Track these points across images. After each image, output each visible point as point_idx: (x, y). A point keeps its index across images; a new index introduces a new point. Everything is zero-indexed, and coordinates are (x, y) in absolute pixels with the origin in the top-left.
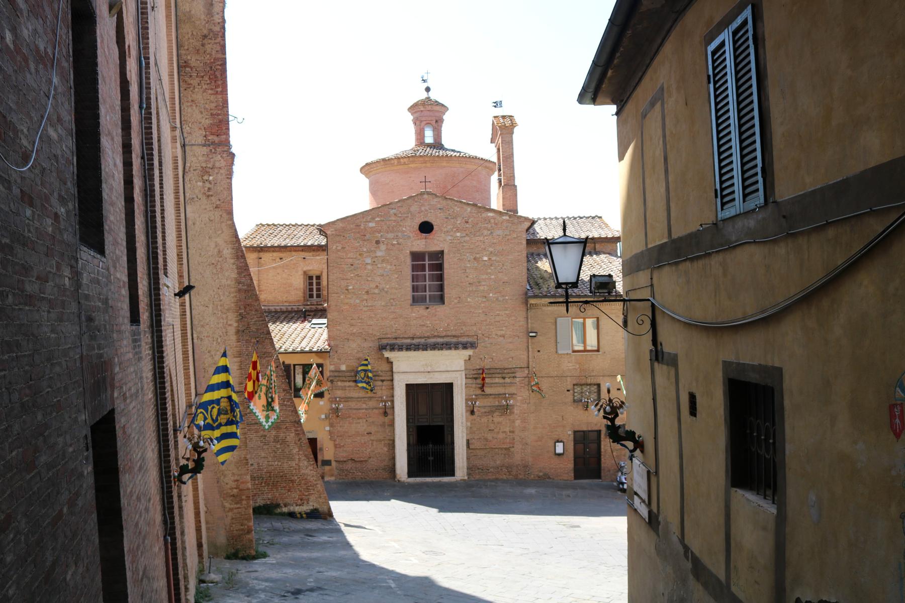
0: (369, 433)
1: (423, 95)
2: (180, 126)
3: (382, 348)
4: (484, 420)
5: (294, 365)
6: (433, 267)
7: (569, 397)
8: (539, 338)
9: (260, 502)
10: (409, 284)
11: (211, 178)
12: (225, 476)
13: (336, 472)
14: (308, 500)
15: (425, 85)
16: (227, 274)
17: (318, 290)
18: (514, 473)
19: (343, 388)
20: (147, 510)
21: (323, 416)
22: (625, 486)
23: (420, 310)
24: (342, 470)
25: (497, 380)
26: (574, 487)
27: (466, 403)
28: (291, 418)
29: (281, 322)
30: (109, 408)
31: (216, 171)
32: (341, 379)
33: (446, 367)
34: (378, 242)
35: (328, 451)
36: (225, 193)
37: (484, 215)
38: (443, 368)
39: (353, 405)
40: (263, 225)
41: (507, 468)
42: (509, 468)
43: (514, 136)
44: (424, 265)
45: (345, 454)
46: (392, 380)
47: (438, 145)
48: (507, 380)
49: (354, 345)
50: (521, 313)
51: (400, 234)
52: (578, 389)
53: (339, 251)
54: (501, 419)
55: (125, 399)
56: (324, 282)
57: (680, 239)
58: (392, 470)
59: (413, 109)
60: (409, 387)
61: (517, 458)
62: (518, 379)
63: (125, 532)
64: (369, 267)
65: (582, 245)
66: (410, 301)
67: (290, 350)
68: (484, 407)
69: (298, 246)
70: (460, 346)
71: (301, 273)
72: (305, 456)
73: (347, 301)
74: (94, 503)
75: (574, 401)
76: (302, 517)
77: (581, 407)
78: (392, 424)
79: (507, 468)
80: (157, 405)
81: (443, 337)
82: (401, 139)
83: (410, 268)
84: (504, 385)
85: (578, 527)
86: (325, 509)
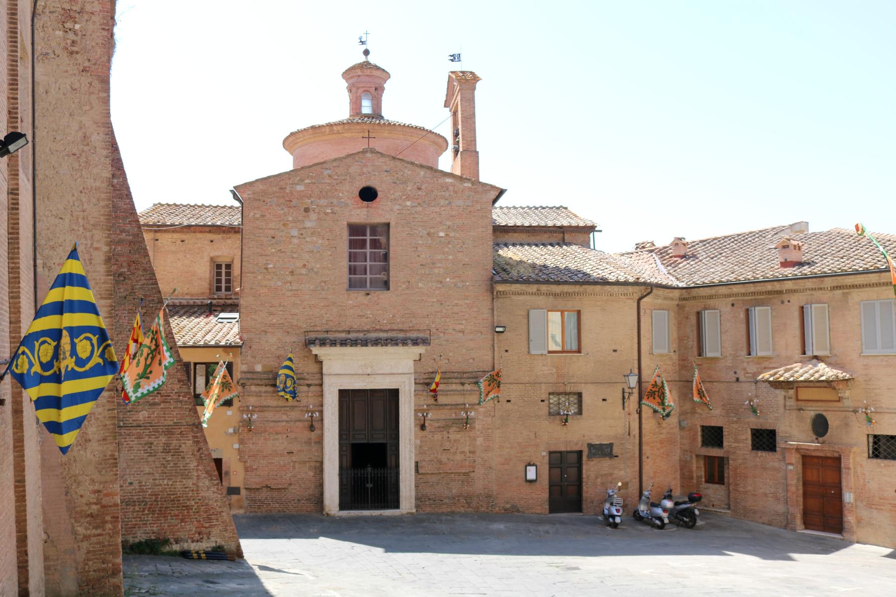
1: (362, 59)
3: (311, 342)
4: (438, 437)
5: (195, 364)
6: (375, 244)
7: (544, 409)
9: (140, 536)
10: (345, 263)
11: (77, 27)
13: (246, 503)
14: (209, 533)
15: (364, 47)
16: (95, 171)
17: (228, 281)
18: (474, 504)
19: (258, 395)
21: (231, 430)
22: (618, 520)
23: (358, 297)
24: (254, 501)
25: (454, 387)
26: (552, 522)
27: (416, 415)
28: (188, 419)
29: (180, 317)
31: (86, 17)
32: (255, 382)
33: (389, 368)
34: (307, 210)
35: (237, 477)
36: (99, 51)
37: (441, 181)
38: (387, 370)
39: (270, 415)
40: (162, 205)
41: (466, 498)
42: (468, 498)
43: (476, 92)
44: (365, 241)
46: (321, 385)
47: (377, 114)
48: (467, 387)
49: (273, 340)
50: (484, 303)
51: (335, 201)
52: (553, 399)
53: (257, 219)
54: (458, 436)
56: (236, 271)
58: (319, 500)
59: (349, 74)
60: (342, 393)
61: (478, 486)
64: (296, 241)
66: (346, 285)
67: (191, 343)
69: (204, 226)
70: (409, 342)
71: (207, 259)
72: (207, 472)
73: (265, 283)
75: (550, 414)
76: (200, 558)
77: (558, 422)
78: (320, 441)
79: (466, 498)
81: (387, 331)
82: (335, 106)
83: (347, 244)
84: (463, 393)
85: (577, 569)
86: (233, 546)
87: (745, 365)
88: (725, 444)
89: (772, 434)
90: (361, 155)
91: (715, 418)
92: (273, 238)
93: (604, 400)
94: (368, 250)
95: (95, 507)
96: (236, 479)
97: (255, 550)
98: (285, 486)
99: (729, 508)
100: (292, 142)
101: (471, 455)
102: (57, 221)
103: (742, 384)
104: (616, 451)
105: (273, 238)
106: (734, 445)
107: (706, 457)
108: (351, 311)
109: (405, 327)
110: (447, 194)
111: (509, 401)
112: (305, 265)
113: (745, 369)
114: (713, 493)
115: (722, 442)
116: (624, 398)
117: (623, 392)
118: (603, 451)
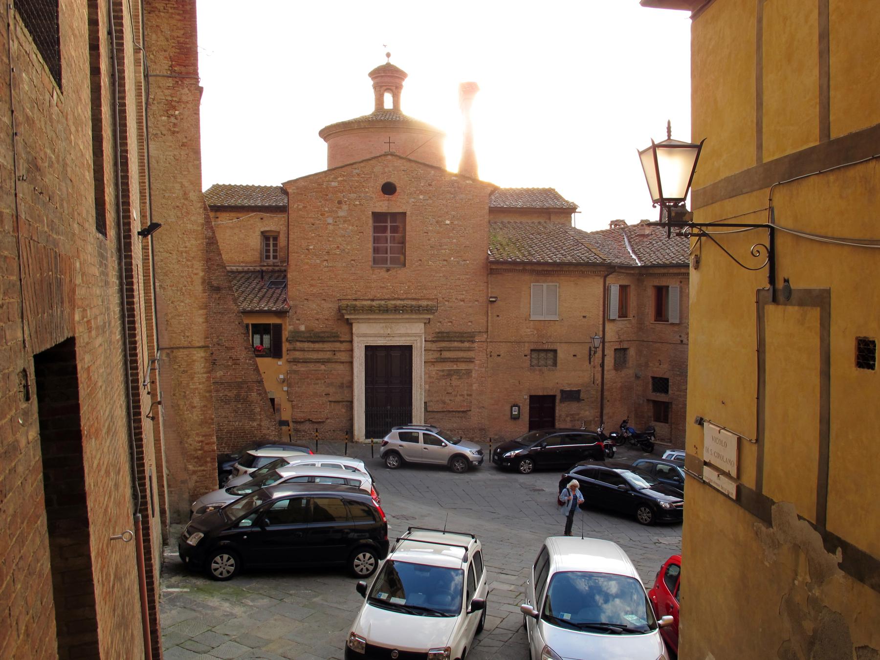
0: (327, 394)
1: (383, 61)
2: (144, 47)
6: (394, 230)
8: (499, 303)
10: (370, 245)
11: (177, 112)
12: (189, 436)
16: (193, 218)
20: (117, 486)
30: (67, 335)
34: (340, 202)
44: (386, 227)
45: (302, 415)
46: (351, 342)
51: (363, 195)
52: (535, 355)
53: (300, 210)
55: (90, 330)
56: (282, 241)
57: (839, 141)
58: (350, 431)
62: (476, 345)
63: (91, 529)
65: (696, 150)
66: (371, 263)
68: (443, 371)
71: (258, 233)
74: (41, 497)
80: (125, 350)
82: (360, 104)
88: (670, 392)
90: (383, 158)
94: (389, 234)
95: (200, 452)
96: (286, 415)
97: (206, 186)
99: (671, 442)
102: (168, 255)
104: (582, 395)
106: (677, 393)
107: (654, 402)
109: (417, 296)
112: (338, 247)
114: (661, 429)
117: (590, 350)
118: (572, 396)
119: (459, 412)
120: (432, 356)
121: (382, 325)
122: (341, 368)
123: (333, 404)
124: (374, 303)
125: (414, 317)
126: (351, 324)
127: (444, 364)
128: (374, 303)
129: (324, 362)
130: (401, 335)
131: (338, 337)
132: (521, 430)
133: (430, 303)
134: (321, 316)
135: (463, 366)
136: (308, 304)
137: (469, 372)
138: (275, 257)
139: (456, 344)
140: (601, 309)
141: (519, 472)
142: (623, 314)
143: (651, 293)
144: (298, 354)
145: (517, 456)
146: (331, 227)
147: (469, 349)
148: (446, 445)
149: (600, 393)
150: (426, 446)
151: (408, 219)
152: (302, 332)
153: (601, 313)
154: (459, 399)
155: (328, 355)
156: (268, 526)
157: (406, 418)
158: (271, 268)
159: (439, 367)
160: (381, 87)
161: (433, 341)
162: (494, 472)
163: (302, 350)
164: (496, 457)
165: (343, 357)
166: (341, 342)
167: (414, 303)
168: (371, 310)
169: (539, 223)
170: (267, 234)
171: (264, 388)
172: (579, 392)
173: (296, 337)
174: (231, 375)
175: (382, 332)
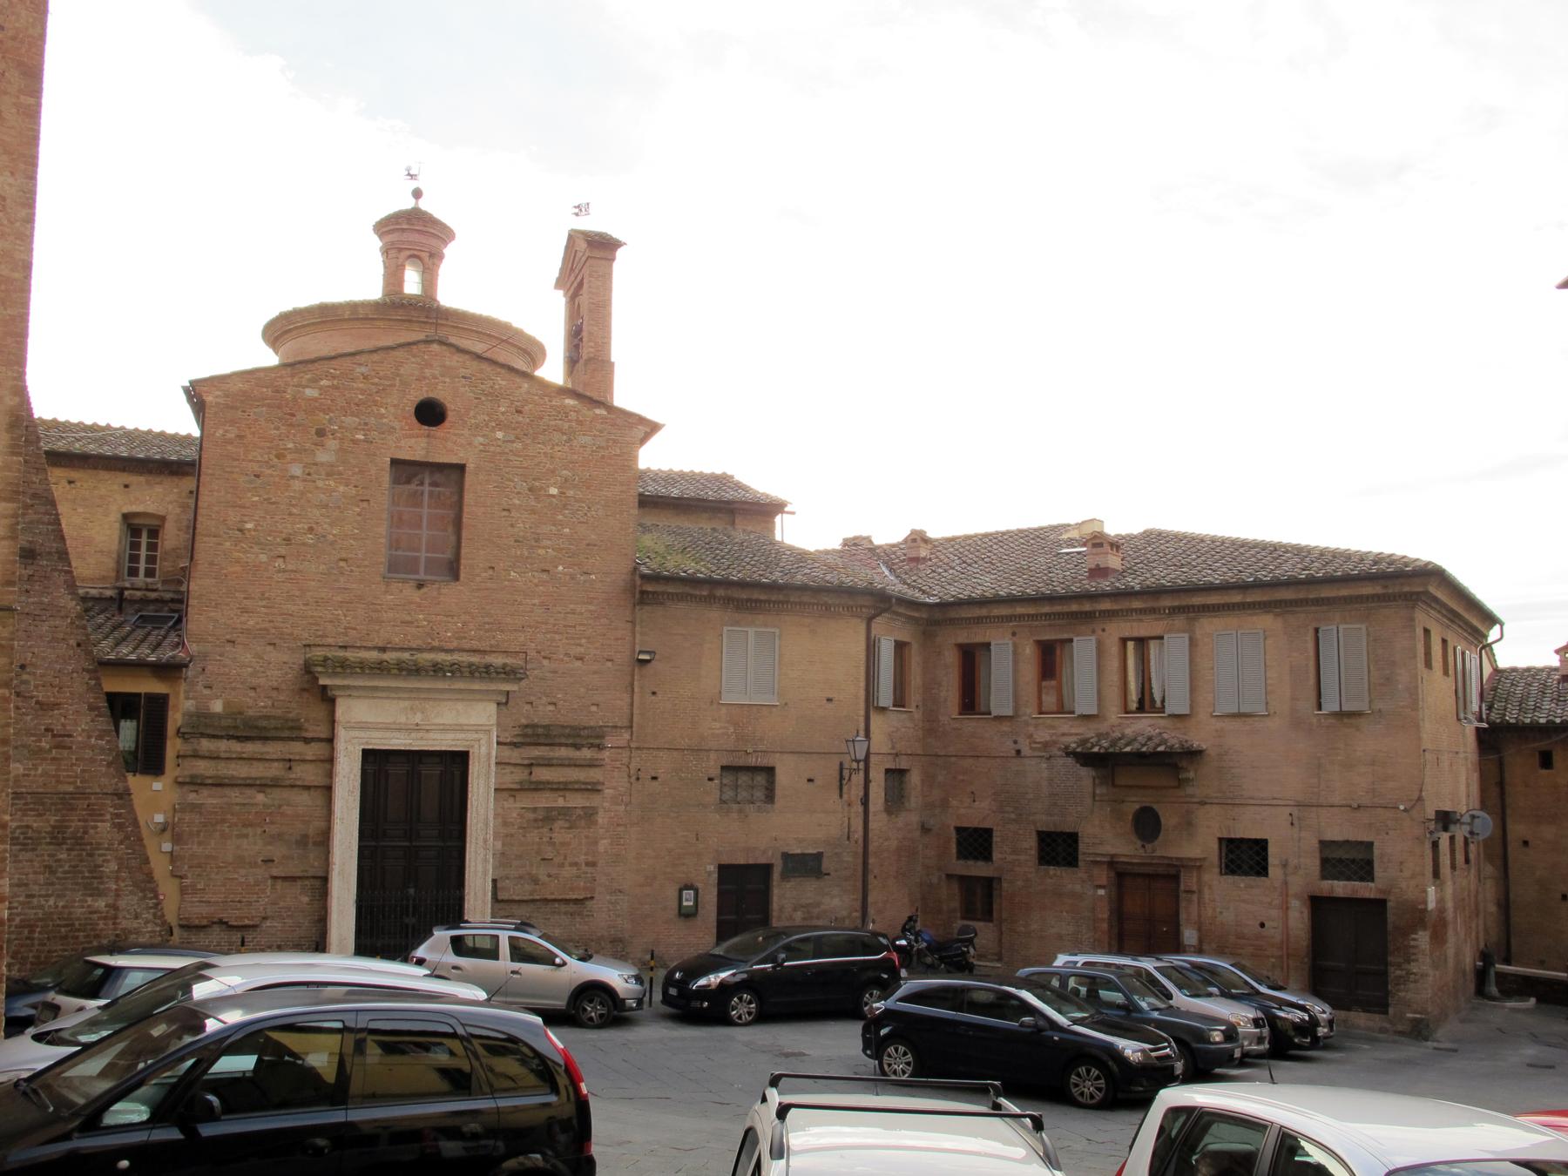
1: (408, 203)
15: (414, 185)
33: (463, 722)
34: (321, 433)
45: (205, 910)
46: (331, 740)
53: (230, 442)
56: (171, 537)
62: (606, 754)
66: (383, 569)
68: (535, 810)
82: (360, 278)
85: (1530, 1065)
87: (1031, 729)
88: (996, 855)
89: (1072, 839)
90: (422, 346)
91: (977, 813)
92: (257, 476)
93: (810, 780)
98: (256, 921)
99: (1000, 960)
100: (197, 395)
101: (589, 869)
103: (1027, 761)
104: (826, 864)
105: (257, 476)
106: (1010, 858)
107: (962, 879)
108: (391, 615)
110: (566, 426)
111: (654, 778)
112: (311, 529)
113: (1031, 736)
115: (990, 854)
116: (842, 778)
118: (806, 865)
119: (567, 901)
120: (515, 777)
121: (402, 704)
122: (304, 800)
123: (279, 884)
124: (386, 656)
125: (476, 686)
126: (332, 701)
127: (536, 795)
128: (386, 656)
129: (263, 786)
130: (445, 729)
131: (300, 728)
132: (701, 938)
133: (509, 661)
134: (262, 681)
135: (577, 801)
136: (232, 657)
137: (589, 814)
138: (150, 573)
139: (563, 752)
140: (863, 684)
141: (726, 1021)
142: (900, 702)
143: (951, 658)
144: (202, 767)
145: (722, 984)
146: (297, 485)
147: (592, 765)
148: (564, 964)
149: (860, 861)
150: (517, 966)
151: (469, 479)
152: (218, 716)
153: (862, 693)
154: (568, 872)
155: (275, 770)
156: (211, 1115)
157: (453, 914)
158: (139, 594)
159: (526, 801)
160: (400, 250)
161: (515, 745)
162: (670, 1024)
163: (214, 757)
164: (673, 991)
165: (310, 774)
166: (307, 741)
167: (475, 659)
168: (380, 669)
169: (714, 530)
170: (136, 521)
171: (132, 810)
172: (819, 856)
173: (202, 725)
174: (45, 774)
175: (403, 719)
